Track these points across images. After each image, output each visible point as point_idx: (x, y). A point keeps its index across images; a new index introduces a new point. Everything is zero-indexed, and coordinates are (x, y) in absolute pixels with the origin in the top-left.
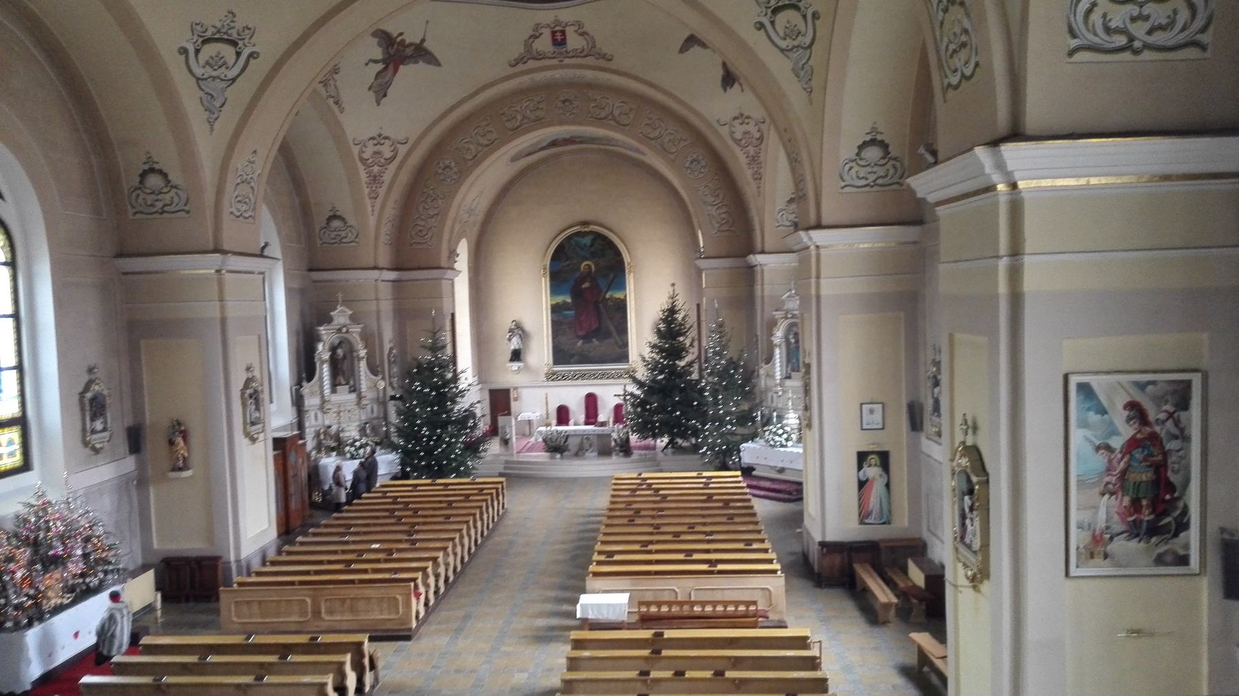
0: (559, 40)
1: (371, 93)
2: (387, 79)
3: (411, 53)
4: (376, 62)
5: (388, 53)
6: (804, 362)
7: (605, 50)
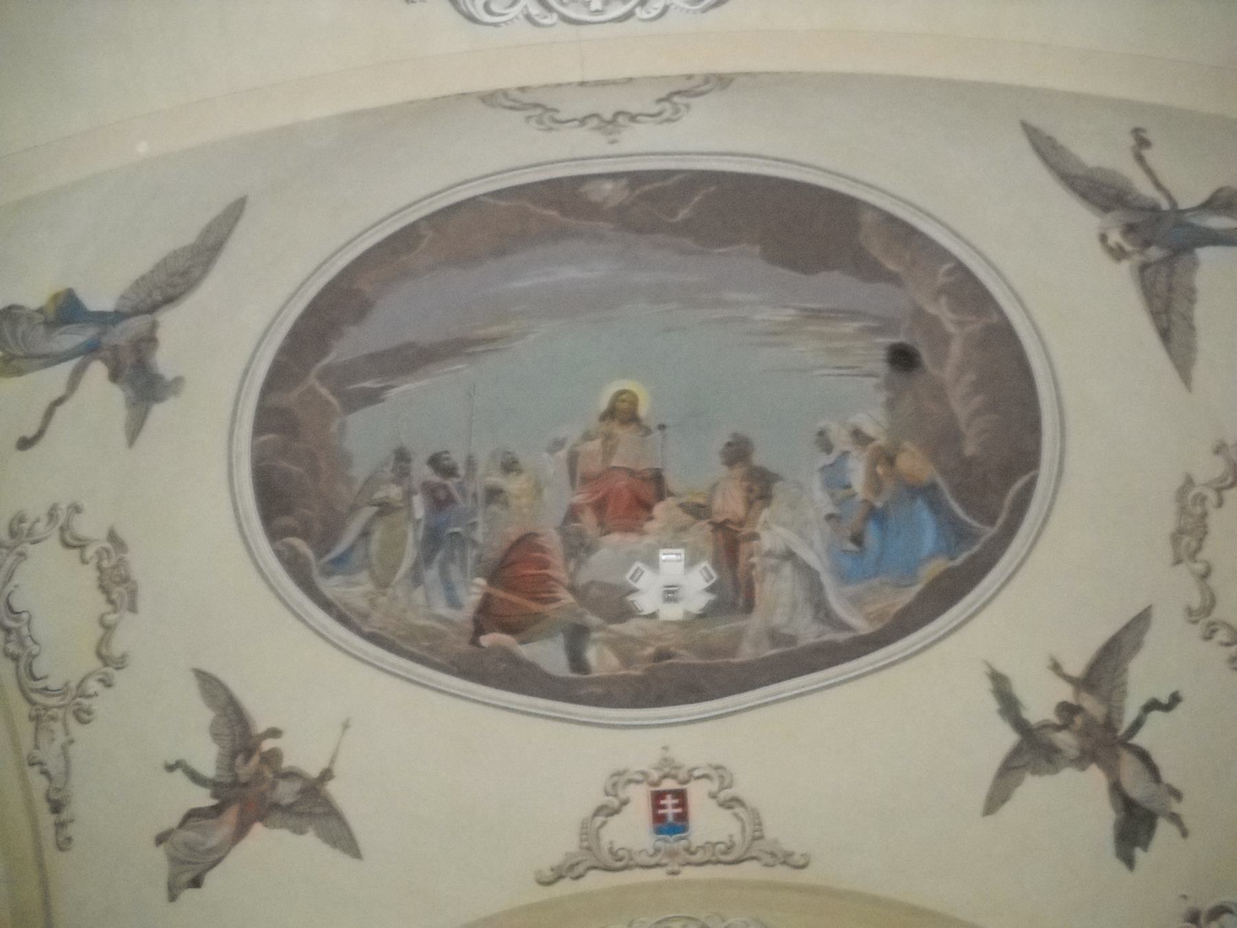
0: (670, 819)
1: (159, 856)
2: (213, 842)
4: (195, 777)
5: (231, 768)
7: (788, 844)
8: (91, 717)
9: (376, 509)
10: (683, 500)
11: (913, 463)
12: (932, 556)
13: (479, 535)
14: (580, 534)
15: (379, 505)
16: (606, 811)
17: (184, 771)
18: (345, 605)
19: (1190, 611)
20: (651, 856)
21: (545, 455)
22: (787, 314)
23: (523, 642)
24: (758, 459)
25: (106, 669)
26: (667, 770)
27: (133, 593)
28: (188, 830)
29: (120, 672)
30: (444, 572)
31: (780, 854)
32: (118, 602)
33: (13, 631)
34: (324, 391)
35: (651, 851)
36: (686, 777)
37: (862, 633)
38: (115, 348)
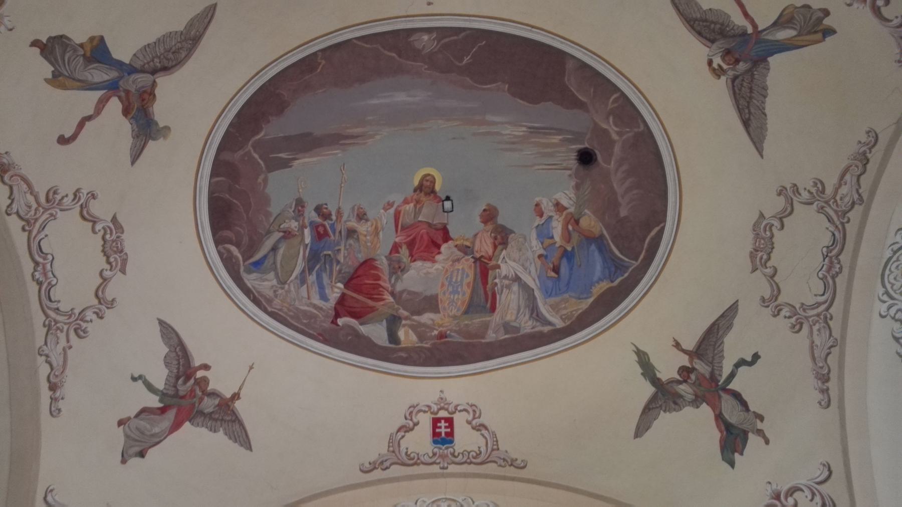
2: (156, 430)
3: (210, 410)
4: (150, 387)
6: (858, 169)
8: (88, 334)
9: (281, 234)
10: (458, 243)
11: (590, 222)
12: (600, 280)
13: (341, 258)
14: (399, 261)
15: (285, 232)
16: (405, 429)
17: (143, 382)
18: (259, 292)
19: (763, 300)
20: (431, 458)
21: (382, 211)
22: (520, 131)
23: (361, 324)
24: (500, 220)
25: (100, 306)
26: (442, 405)
27: (124, 262)
28: (141, 420)
29: (110, 310)
30: (319, 277)
31: (509, 460)
32: (114, 264)
33: (41, 265)
34: (256, 156)
35: (431, 455)
36: (454, 410)
37: (558, 327)
38: (127, 92)
